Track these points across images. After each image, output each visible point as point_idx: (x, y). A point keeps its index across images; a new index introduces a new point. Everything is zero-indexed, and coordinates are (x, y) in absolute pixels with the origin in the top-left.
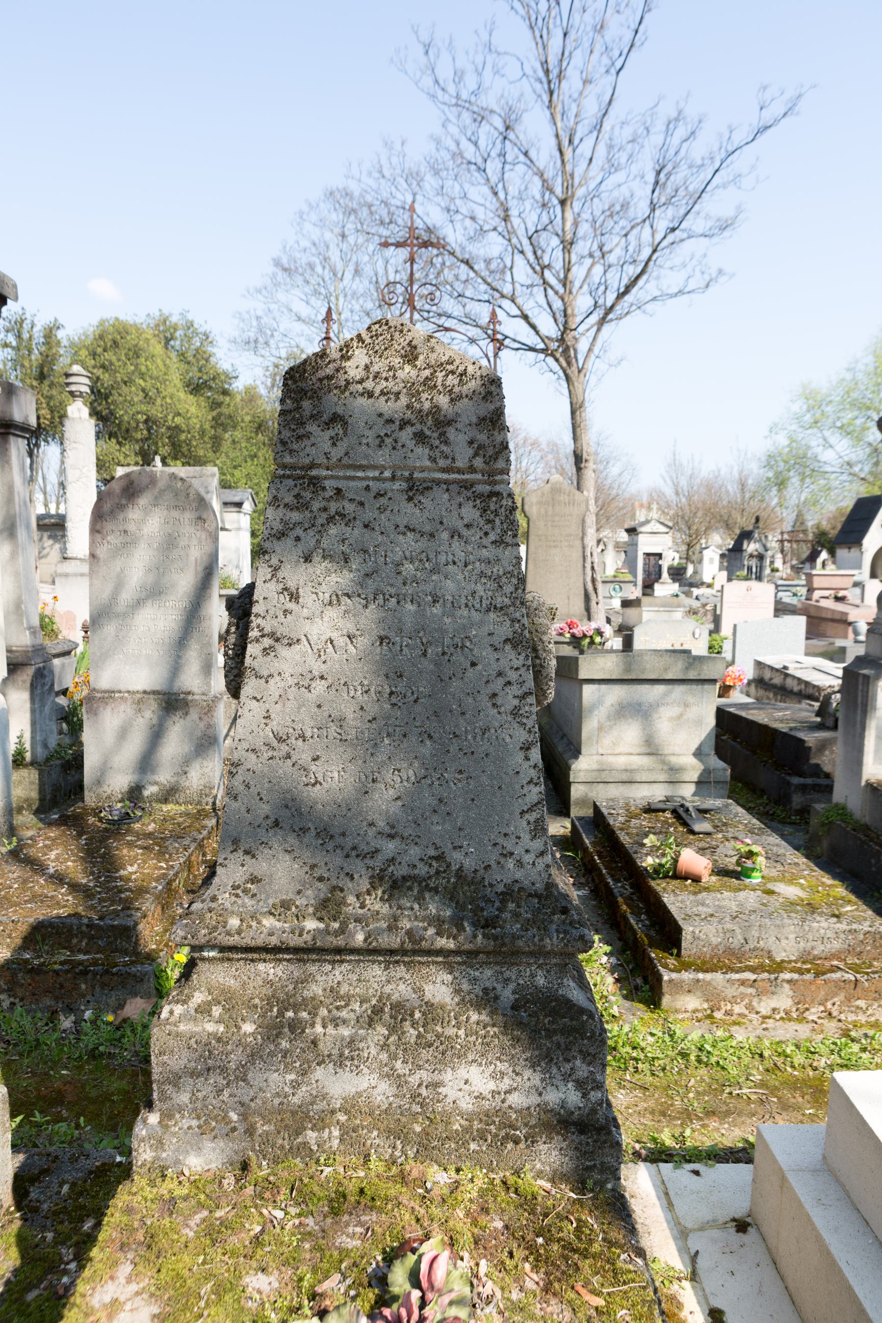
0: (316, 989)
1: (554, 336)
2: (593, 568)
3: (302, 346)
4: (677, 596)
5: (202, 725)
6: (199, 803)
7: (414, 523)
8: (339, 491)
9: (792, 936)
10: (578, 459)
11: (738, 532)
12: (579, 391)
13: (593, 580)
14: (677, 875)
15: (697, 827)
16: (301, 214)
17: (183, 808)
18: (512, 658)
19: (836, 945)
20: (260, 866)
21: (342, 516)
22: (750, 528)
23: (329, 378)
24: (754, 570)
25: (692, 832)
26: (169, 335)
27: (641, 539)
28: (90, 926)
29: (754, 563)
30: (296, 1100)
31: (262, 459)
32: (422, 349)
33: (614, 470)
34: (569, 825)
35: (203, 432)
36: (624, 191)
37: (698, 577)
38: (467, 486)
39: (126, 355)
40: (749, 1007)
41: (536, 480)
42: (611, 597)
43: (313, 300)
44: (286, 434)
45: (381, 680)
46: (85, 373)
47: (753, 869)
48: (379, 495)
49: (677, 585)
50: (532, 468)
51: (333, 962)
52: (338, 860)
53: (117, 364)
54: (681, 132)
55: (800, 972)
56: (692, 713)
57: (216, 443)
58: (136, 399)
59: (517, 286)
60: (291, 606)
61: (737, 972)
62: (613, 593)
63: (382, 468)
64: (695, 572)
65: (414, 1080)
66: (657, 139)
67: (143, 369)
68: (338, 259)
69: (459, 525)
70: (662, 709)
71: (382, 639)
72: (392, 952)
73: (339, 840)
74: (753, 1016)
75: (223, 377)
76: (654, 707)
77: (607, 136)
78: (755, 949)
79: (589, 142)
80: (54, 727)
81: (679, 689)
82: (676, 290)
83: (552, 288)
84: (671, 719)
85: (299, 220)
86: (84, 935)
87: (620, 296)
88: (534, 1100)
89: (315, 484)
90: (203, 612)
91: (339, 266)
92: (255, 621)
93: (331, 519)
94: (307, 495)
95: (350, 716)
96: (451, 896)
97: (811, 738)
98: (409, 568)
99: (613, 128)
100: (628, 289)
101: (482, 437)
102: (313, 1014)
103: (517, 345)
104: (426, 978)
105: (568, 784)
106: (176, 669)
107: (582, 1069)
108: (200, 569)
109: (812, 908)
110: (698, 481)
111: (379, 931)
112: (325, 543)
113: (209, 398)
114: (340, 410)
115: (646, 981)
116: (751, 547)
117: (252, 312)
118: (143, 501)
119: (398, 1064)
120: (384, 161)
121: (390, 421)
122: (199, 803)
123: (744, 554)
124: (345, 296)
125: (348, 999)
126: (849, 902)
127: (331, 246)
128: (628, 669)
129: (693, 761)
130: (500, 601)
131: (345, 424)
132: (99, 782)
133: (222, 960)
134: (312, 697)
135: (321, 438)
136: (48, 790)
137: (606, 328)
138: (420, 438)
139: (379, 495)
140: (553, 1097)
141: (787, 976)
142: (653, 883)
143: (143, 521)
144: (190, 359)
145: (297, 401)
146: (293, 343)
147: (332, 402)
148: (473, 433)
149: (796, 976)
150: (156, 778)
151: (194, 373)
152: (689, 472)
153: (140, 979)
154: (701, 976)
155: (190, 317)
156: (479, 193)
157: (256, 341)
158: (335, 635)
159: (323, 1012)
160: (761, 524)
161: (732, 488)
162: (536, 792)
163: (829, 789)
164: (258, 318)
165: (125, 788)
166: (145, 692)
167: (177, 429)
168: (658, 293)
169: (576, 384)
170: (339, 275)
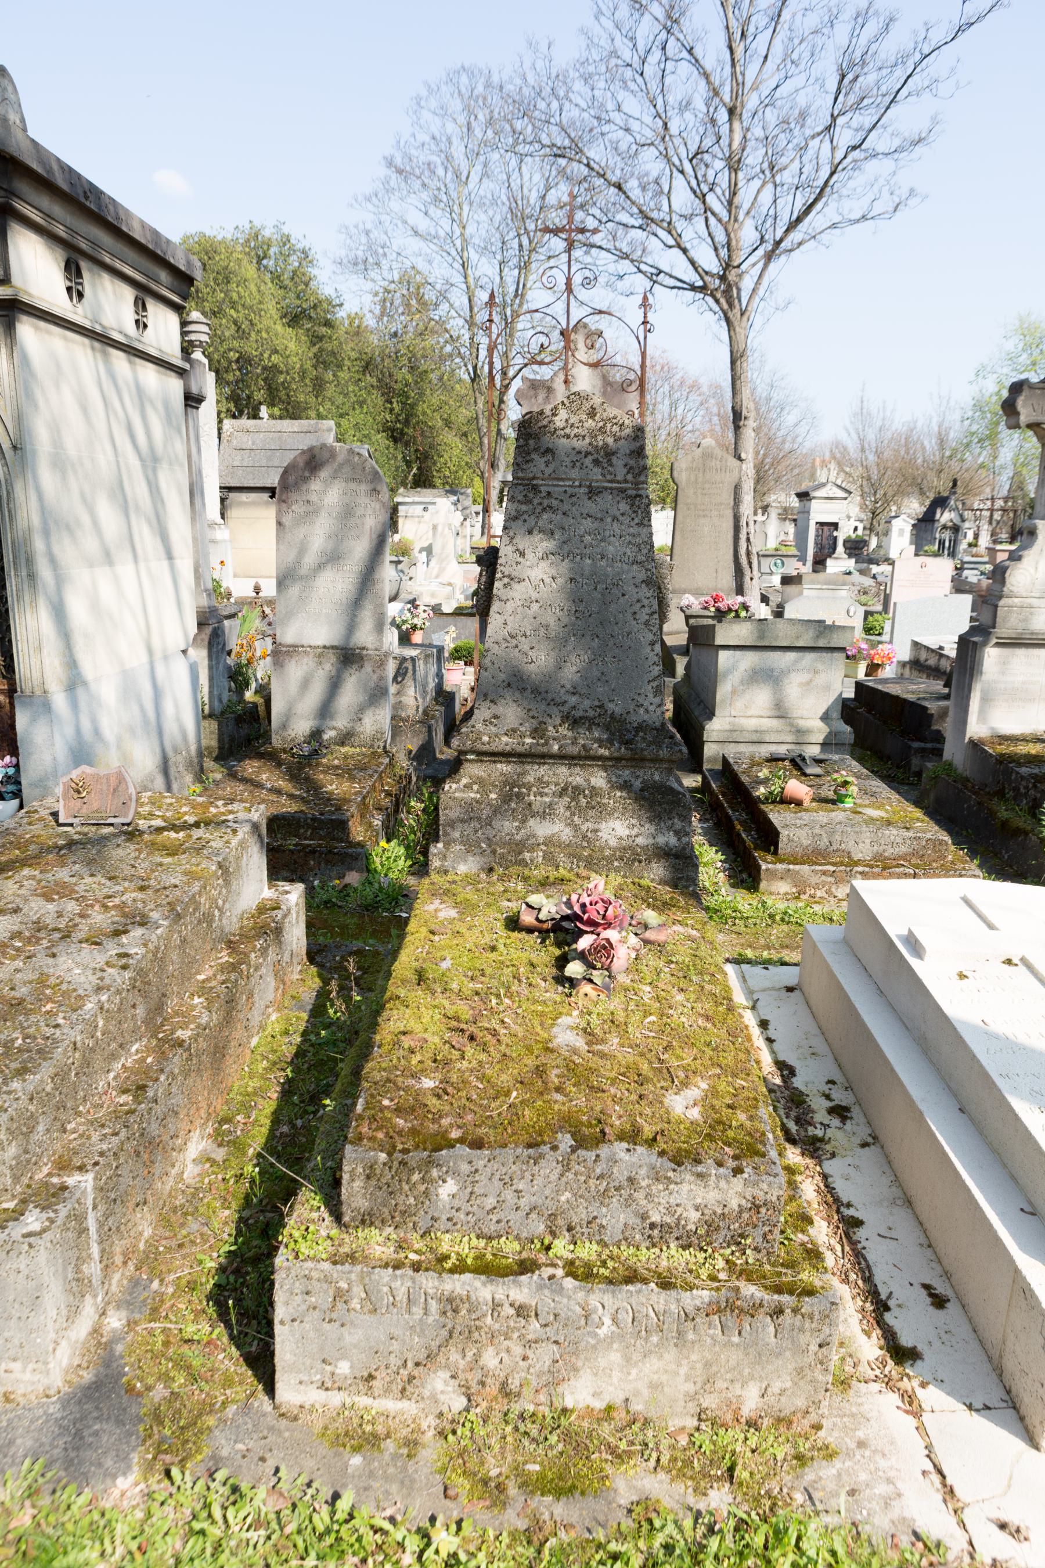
0: (530, 778)
1: (715, 271)
2: (748, 540)
3: (420, 267)
4: (849, 573)
5: (375, 677)
6: (372, 746)
7: (591, 512)
8: (549, 493)
9: (868, 841)
10: (737, 416)
11: (932, 496)
12: (741, 337)
13: (748, 554)
14: (784, 800)
15: (808, 771)
16: (418, 100)
17: (358, 750)
18: (646, 592)
19: (903, 849)
20: (499, 709)
21: (551, 508)
22: (946, 494)
23: (545, 427)
24: (947, 544)
25: (805, 775)
26: (260, 253)
27: (815, 505)
28: (314, 819)
29: (947, 535)
30: (518, 837)
31: (371, 405)
32: (599, 410)
33: (790, 419)
34: (699, 778)
35: (303, 373)
36: (802, 100)
37: (882, 552)
38: (623, 491)
39: (215, 279)
40: (829, 892)
41: (692, 431)
42: (771, 573)
43: (432, 210)
44: (520, 459)
45: (570, 603)
46: (205, 320)
47: (846, 796)
48: (572, 496)
49: (853, 560)
50: (690, 415)
51: (539, 764)
52: (543, 706)
53: (205, 291)
54: (872, 27)
55: (871, 866)
56: (821, 679)
57: (319, 385)
58: (227, 334)
59: (674, 216)
60: (520, 559)
61: (822, 864)
62: (774, 569)
63: (574, 480)
64: (879, 546)
65: (584, 828)
66: (842, 33)
67: (235, 296)
68: (462, 157)
69: (618, 513)
70: (793, 675)
71: (571, 579)
72: (573, 758)
73: (544, 695)
74: (832, 899)
75: (325, 306)
76: (786, 672)
77: (786, 26)
78: (838, 850)
79: (764, 37)
80: (226, 684)
81: (809, 657)
82: (858, 217)
83: (714, 214)
84: (801, 685)
85: (415, 107)
86: (309, 826)
87: (792, 226)
88: (651, 841)
89: (535, 489)
90: (377, 576)
91: (464, 166)
92: (499, 568)
93: (544, 510)
94: (531, 495)
95: (552, 624)
96: (607, 728)
97: (933, 707)
98: (588, 539)
99: (794, 15)
100: (799, 220)
101: (632, 462)
102: (529, 790)
103: (673, 282)
104: (592, 774)
105: (703, 743)
106: (351, 627)
107: (678, 824)
108: (374, 536)
109: (889, 823)
110: (889, 435)
111: (567, 745)
112: (540, 523)
113: (308, 330)
114: (550, 446)
115: (750, 876)
116: (945, 517)
117: (361, 226)
118: (324, 474)
119: (576, 818)
120: (527, 65)
121: (579, 452)
122: (372, 746)
123: (936, 525)
124: (471, 204)
125: (548, 784)
126: (918, 820)
127: (454, 139)
128: (761, 637)
129: (820, 724)
130: (640, 558)
131: (553, 454)
132: (284, 726)
133: (477, 761)
134: (531, 612)
135: (540, 462)
136: (227, 740)
137: (772, 266)
138: (596, 462)
139: (572, 496)
140: (661, 840)
141: (860, 869)
142: (762, 807)
143: (324, 492)
144: (287, 282)
145: (526, 440)
146: (408, 264)
147: (547, 440)
148: (627, 460)
149: (867, 869)
150: (334, 723)
151: (291, 300)
152: (879, 423)
153: (355, 858)
154: (791, 867)
155: (286, 230)
156: (633, 105)
157: (365, 261)
158: (545, 577)
159: (534, 789)
160: (959, 490)
161: (930, 445)
162: (657, 670)
163: (939, 752)
164: (367, 233)
165: (307, 732)
166: (325, 647)
167: (274, 369)
168: (837, 219)
169: (738, 329)
170: (464, 179)
